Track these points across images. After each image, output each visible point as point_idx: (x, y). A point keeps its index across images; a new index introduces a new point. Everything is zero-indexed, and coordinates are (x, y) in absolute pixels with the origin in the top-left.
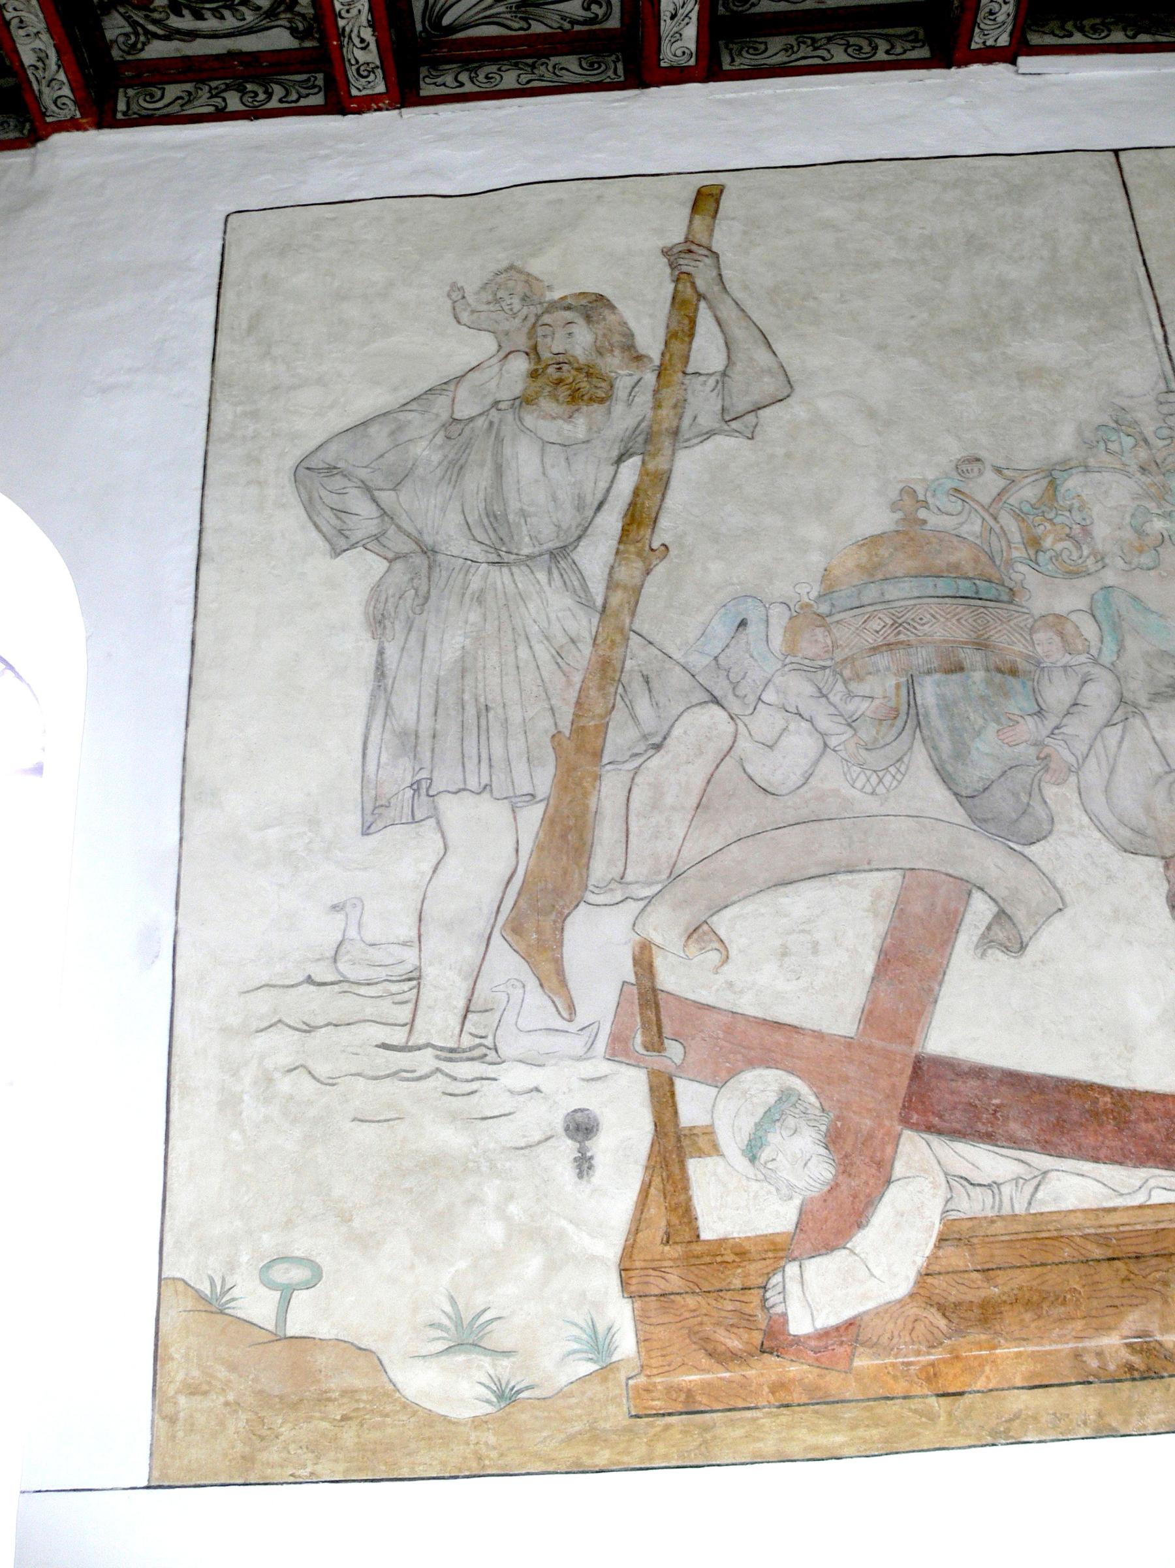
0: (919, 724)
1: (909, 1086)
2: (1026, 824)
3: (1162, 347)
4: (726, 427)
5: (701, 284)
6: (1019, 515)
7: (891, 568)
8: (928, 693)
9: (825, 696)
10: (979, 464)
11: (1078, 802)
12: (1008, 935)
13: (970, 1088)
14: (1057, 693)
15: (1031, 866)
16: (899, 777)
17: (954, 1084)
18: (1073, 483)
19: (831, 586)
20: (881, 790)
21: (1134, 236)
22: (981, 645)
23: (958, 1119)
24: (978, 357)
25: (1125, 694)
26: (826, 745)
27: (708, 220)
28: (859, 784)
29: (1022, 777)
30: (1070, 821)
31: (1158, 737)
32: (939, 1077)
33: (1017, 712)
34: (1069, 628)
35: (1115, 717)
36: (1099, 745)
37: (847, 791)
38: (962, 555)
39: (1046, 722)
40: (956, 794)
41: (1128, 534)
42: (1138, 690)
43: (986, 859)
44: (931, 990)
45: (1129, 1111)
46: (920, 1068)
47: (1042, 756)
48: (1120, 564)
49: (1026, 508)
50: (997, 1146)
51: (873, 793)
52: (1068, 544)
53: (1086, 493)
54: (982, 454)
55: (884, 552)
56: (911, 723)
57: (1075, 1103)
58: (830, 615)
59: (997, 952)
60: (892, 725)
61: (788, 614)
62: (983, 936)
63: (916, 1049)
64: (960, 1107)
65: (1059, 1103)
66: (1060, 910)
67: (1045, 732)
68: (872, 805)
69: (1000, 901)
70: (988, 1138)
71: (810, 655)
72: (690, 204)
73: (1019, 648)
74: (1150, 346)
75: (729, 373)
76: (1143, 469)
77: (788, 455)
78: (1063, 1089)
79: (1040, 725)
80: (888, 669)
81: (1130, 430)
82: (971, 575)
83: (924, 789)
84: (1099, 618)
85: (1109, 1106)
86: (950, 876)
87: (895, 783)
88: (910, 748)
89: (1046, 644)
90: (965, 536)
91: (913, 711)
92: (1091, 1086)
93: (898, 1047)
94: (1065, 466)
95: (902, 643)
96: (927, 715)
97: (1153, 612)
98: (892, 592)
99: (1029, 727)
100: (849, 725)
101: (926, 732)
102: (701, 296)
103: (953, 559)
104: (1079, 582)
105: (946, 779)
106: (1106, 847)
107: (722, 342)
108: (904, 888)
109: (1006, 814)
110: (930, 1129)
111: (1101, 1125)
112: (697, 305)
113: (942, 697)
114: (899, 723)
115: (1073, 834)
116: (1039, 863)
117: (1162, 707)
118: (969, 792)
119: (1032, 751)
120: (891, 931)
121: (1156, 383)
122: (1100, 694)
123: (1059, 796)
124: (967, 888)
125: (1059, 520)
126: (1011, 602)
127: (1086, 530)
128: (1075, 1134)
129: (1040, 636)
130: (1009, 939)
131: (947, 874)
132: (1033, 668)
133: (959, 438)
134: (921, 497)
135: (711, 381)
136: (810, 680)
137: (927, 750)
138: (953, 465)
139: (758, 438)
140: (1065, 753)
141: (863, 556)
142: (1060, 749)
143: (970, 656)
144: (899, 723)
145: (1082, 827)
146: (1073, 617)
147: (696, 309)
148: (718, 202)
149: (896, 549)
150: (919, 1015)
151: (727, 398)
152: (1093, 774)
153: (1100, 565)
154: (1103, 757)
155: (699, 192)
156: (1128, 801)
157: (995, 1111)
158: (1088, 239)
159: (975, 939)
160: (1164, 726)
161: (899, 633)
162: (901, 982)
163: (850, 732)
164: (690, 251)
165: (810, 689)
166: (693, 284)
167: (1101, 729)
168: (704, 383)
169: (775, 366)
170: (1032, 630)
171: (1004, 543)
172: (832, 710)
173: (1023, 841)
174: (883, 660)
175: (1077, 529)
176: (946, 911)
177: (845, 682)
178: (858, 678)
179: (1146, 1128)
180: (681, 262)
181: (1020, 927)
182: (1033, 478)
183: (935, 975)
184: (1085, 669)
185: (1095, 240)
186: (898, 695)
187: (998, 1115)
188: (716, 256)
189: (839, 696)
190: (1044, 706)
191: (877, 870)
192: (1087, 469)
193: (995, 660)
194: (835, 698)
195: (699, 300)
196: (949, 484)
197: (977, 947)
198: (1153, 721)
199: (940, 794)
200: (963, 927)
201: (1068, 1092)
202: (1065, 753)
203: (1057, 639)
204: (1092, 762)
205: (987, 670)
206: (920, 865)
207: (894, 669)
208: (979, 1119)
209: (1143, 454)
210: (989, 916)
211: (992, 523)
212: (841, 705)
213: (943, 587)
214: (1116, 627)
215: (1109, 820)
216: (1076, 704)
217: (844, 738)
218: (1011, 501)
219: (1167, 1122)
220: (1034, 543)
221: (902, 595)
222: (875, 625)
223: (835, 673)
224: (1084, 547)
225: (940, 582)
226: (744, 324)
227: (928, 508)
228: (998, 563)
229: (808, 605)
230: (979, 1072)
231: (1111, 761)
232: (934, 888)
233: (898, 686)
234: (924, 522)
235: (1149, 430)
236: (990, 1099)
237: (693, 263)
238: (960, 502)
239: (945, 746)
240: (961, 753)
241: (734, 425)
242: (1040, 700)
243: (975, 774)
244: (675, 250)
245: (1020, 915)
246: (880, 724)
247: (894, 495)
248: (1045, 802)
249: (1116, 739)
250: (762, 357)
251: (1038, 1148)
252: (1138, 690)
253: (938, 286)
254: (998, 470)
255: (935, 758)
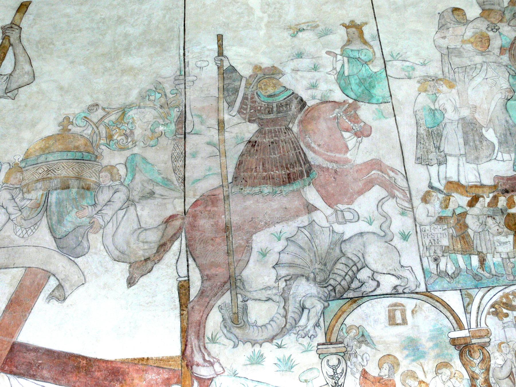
0: (47, 209)
1: (7, 355)
2: (79, 249)
3: (182, 58)
4: (5, 95)
5: (12, 40)
6: (107, 127)
7: (52, 148)
8: (53, 197)
9: (14, 199)
10: (97, 107)
11: (101, 240)
12: (60, 295)
13: (30, 356)
14: (103, 197)
15: (75, 266)
16: (34, 231)
17: (25, 354)
18: (132, 113)
19: (28, 156)
20: (26, 236)
21: (183, 14)
22: (78, 178)
23: (23, 369)
24: (109, 65)
25: (130, 197)
26: (9, 218)
27: (22, 15)
28: (18, 234)
29: (81, 230)
30: (96, 248)
31: (139, 214)
32: (20, 351)
33: (86, 204)
34: (115, 171)
35: (124, 206)
36: (114, 218)
37: (13, 236)
38: (81, 142)
39: (96, 208)
40: (54, 237)
41: (148, 133)
42: (136, 195)
43: (59, 264)
44: (26, 316)
45: (92, 367)
46: (13, 347)
47: (91, 222)
48: (142, 144)
49: (111, 123)
50: (36, 380)
51: (23, 237)
52: (123, 137)
53: (136, 117)
54: (100, 103)
55: (51, 142)
56: (44, 209)
57: (71, 363)
58: (25, 167)
59: (54, 300)
60: (36, 210)
61: (9, 167)
62: (50, 294)
63: (14, 340)
64: (25, 364)
65: (64, 363)
66: (83, 284)
67: (95, 212)
68: (22, 242)
69: (60, 280)
70: (33, 377)
71: (13, 183)
72: (16, 9)
73: (94, 179)
74: (177, 57)
75: (13, 74)
76: (161, 107)
77: (26, 106)
78: (67, 357)
79: (93, 210)
80: (41, 188)
81: (160, 91)
82: (82, 150)
83: (43, 236)
84: (127, 166)
85: (85, 364)
86: (44, 270)
87: (32, 233)
88: (41, 220)
89: (105, 178)
90: (85, 135)
91: (45, 205)
92: (79, 356)
93: (7, 339)
94: (130, 106)
95: (48, 178)
96: (50, 206)
97: (149, 164)
98: (51, 158)
99: (89, 211)
100: (20, 210)
101: (48, 213)
102: (11, 45)
103: (76, 144)
104: (123, 152)
105: (52, 230)
106: (108, 259)
107: (13, 62)
108: (25, 275)
109: (70, 246)
110: (11, 373)
111: (79, 372)
112: (8, 49)
113: (58, 199)
114: (39, 209)
115: (96, 254)
116: (79, 265)
117: (144, 202)
118: (60, 237)
119: (88, 220)
120: (16, 292)
121: (176, 72)
122: (120, 197)
123: (95, 239)
124: (48, 274)
125: (122, 128)
126: (95, 161)
127: (132, 132)
128: (68, 376)
129: (102, 174)
130: (60, 296)
131: (42, 269)
132: (97, 187)
133: (92, 96)
134: (71, 120)
135: (5, 78)
136: (10, 193)
137: (48, 220)
138: (87, 108)
139: (16, 99)
140: (101, 221)
141: (42, 145)
142: (98, 219)
143: (74, 183)
144: (39, 209)
145: (100, 250)
146: (118, 166)
147: (8, 50)
148: (27, 8)
149: (56, 141)
150: (18, 326)
151: (9, 85)
152: (110, 229)
153: (134, 145)
154: (115, 223)
155: (22, 4)
156: (120, 240)
157: (39, 366)
158: (164, 17)
159: (47, 296)
160: (142, 210)
161: (48, 174)
162: (14, 313)
163: (20, 213)
164: (12, 27)
165: (9, 196)
166: (9, 40)
167: (117, 211)
168: (2, 78)
169: (31, 71)
170: (100, 172)
171: (98, 137)
172: (15, 205)
173: (75, 256)
174: (39, 185)
175: (128, 131)
176: (38, 284)
177: (23, 193)
178: (29, 192)
179: (97, 374)
180: (7, 31)
181: (66, 291)
182: (116, 112)
183: (28, 309)
184: (117, 187)
185: (167, 16)
186: (41, 198)
187: (40, 367)
188: (21, 28)
189: (18, 200)
190: (97, 202)
191: (16, 267)
192: (139, 107)
193: (83, 184)
194: (17, 200)
195: (10, 46)
196: (83, 115)
197: (47, 298)
198: (138, 209)
199: (48, 238)
200: (43, 291)
201: (69, 358)
202: (101, 221)
203: (109, 175)
204: (110, 224)
205: (78, 188)
206: (33, 266)
207: (43, 188)
208: (32, 369)
209: (163, 100)
210: (55, 286)
211: (95, 129)
212: (18, 203)
213: (70, 155)
214: (134, 171)
215: (111, 248)
216: (109, 201)
217: (18, 215)
218: (105, 121)
219: (106, 372)
220: (110, 137)
221: (54, 159)
222: (40, 171)
223: (20, 190)
224: (129, 138)
225: (69, 154)
226: (24, 55)
227: (73, 125)
228: (94, 145)
229: (17, 164)
230: (36, 349)
231: (118, 224)
232: (36, 275)
233: (43, 195)
234: (70, 130)
235: (168, 91)
236: (38, 360)
237: (11, 32)
238: (85, 122)
239: (55, 218)
240: (60, 221)
241: (8, 94)
242: (96, 200)
243: (62, 230)
244: (6, 27)
245: (67, 286)
246: (32, 210)
247: (61, 119)
248: (88, 240)
249: (123, 215)
250: (27, 68)
251: (52, 381)
252: (136, 195)
253: (101, 37)
254: (104, 109)
255: (50, 223)
